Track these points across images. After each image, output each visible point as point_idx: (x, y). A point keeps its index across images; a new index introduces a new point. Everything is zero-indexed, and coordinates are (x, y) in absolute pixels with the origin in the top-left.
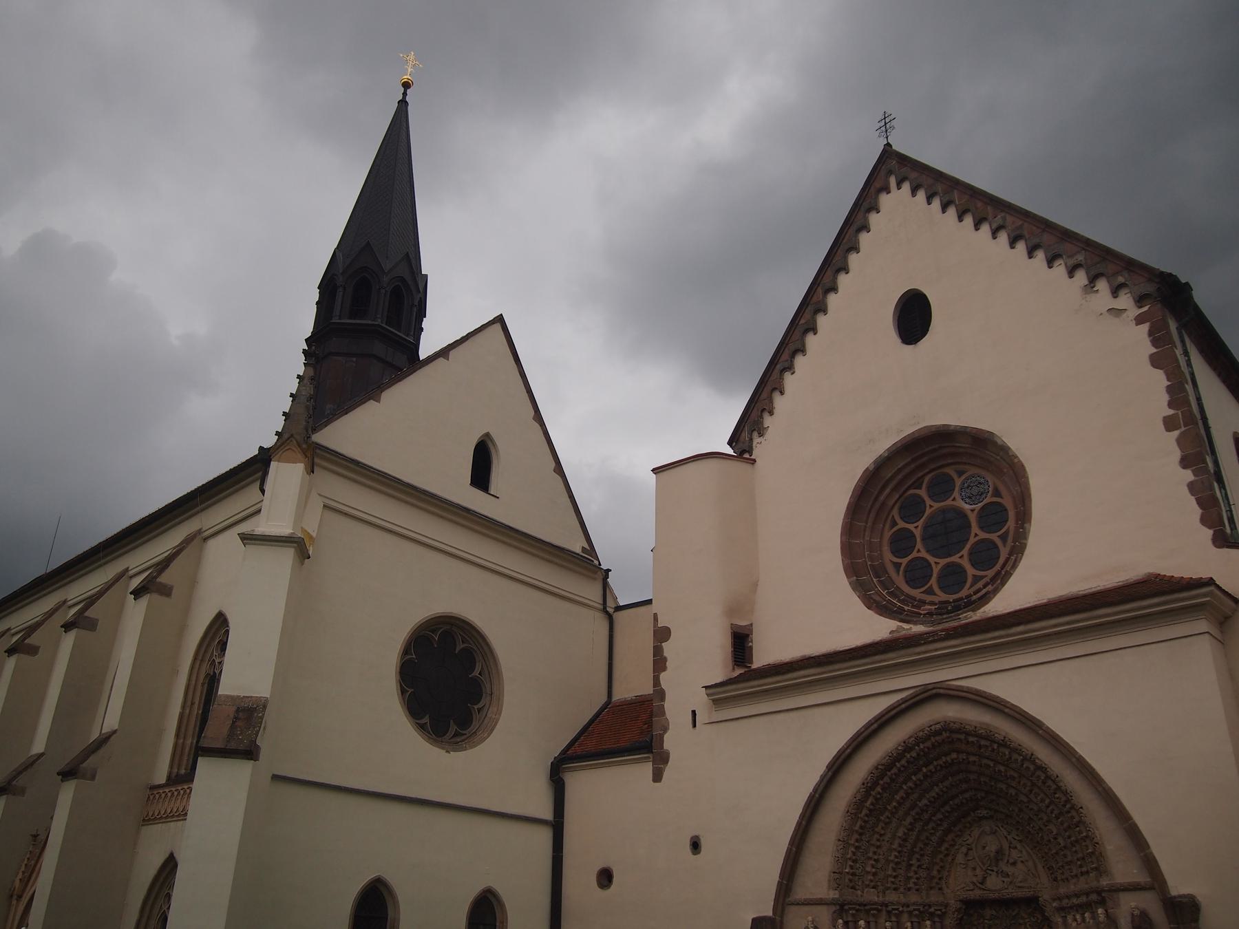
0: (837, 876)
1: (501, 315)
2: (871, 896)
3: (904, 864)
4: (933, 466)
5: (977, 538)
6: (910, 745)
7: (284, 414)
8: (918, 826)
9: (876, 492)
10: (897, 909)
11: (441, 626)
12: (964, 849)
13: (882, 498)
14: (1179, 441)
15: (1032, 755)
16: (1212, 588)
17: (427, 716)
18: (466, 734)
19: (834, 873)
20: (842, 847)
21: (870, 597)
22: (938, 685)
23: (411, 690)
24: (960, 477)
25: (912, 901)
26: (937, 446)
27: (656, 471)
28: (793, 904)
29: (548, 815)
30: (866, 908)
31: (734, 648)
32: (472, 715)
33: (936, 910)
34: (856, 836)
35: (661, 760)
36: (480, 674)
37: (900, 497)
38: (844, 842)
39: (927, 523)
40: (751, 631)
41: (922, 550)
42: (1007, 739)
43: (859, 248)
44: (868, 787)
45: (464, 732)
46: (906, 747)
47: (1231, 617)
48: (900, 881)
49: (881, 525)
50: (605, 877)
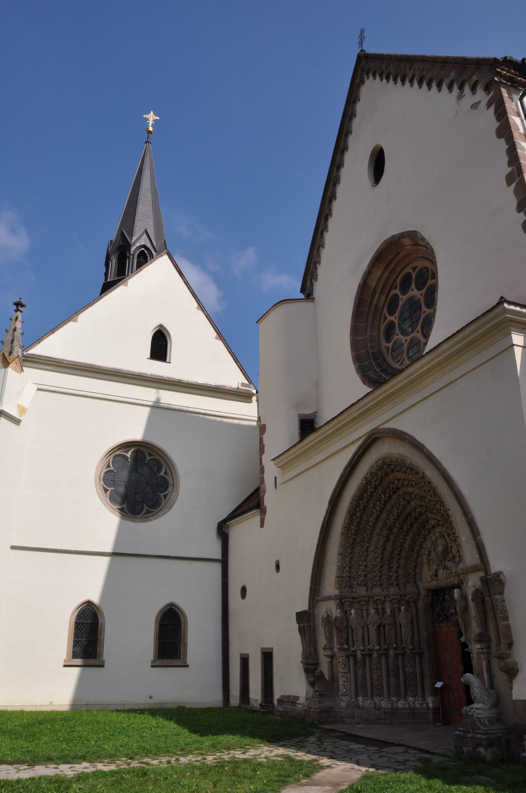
0: (339, 579)
2: (362, 591)
3: (386, 566)
4: (399, 269)
8: (392, 537)
10: (380, 600)
12: (427, 552)
13: (375, 302)
14: (516, 192)
15: (424, 473)
17: (126, 503)
19: (337, 577)
20: (341, 558)
24: (414, 271)
30: (358, 600)
31: (301, 430)
35: (263, 512)
36: (166, 473)
37: (387, 297)
39: (401, 312)
40: (316, 417)
42: (411, 464)
43: (352, 130)
44: (352, 513)
48: (384, 579)
49: (378, 322)
50: (244, 591)
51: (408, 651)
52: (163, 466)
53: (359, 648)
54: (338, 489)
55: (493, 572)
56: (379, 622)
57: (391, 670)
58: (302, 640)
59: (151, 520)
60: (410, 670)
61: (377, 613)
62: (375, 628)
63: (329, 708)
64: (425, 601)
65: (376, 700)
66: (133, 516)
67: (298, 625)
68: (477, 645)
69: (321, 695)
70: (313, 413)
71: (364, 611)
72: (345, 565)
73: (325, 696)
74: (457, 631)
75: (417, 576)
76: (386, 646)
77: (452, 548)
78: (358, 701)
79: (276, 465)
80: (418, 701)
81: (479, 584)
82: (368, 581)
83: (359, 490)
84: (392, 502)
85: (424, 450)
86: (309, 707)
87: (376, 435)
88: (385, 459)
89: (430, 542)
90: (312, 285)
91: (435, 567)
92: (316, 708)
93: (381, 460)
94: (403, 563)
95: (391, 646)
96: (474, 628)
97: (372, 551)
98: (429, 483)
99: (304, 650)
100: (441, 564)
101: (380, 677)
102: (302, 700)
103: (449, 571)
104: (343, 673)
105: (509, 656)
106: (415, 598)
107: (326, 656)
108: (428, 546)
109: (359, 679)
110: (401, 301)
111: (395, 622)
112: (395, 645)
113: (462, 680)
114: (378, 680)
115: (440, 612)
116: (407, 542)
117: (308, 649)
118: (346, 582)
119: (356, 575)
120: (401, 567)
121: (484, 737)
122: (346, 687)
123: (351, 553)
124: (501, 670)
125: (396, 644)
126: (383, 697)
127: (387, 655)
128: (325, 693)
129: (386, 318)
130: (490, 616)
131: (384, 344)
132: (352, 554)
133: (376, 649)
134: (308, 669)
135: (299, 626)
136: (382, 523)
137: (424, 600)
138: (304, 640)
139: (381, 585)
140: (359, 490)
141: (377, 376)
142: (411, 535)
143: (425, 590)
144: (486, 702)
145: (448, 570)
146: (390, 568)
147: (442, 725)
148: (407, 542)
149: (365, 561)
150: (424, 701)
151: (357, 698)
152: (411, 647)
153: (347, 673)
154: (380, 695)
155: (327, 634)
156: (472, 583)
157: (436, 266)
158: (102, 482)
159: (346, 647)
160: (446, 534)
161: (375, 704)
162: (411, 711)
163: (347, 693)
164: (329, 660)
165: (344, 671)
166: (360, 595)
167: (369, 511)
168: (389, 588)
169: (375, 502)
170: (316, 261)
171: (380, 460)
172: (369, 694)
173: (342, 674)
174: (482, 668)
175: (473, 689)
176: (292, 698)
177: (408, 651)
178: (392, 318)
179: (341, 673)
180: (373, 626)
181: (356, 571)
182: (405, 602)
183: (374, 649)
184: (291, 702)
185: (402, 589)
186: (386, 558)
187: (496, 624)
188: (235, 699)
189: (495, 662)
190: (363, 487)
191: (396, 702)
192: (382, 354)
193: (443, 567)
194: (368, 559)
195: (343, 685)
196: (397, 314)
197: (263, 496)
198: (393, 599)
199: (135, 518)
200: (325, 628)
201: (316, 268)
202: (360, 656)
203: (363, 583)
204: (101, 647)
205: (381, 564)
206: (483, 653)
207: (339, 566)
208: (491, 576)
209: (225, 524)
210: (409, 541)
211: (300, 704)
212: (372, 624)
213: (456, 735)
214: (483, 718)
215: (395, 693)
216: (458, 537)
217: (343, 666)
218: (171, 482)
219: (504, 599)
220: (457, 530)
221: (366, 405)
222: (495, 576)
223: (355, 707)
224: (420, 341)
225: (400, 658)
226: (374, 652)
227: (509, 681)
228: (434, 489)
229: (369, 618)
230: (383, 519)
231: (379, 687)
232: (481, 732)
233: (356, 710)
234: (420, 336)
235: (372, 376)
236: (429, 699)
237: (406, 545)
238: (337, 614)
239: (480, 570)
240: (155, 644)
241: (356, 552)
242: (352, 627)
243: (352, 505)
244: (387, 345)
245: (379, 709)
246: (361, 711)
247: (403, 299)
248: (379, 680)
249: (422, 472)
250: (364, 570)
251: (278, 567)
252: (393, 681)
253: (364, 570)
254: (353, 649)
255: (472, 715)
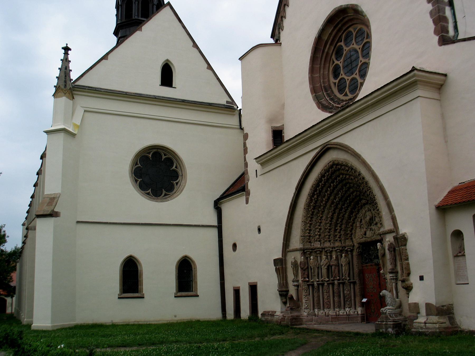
1: (169, 2)
2: (317, 245)
3: (333, 229)
4: (344, 28)
5: (362, 62)
6: (323, 174)
7: (57, 77)
8: (337, 211)
9: (322, 48)
10: (329, 250)
11: (152, 150)
12: (359, 220)
13: (326, 50)
15: (360, 172)
16: (415, 72)
17: (150, 189)
18: (171, 194)
19: (301, 236)
20: (304, 224)
21: (320, 103)
22: (327, 144)
23: (140, 180)
25: (336, 246)
26: (342, 18)
27: (241, 59)
28: (289, 252)
29: (216, 224)
30: (315, 250)
32: (174, 186)
33: (349, 249)
34: (309, 219)
35: (248, 194)
36: (176, 167)
37: (335, 47)
38: (305, 222)
40: (284, 128)
41: (343, 74)
42: (352, 165)
44: (311, 196)
45: (170, 193)
46: (322, 175)
47: (444, 84)
49: (328, 65)
50: (235, 246)
51: (347, 281)
52: (175, 163)
53: (315, 281)
54: (302, 180)
55: (401, 233)
56: (328, 264)
57: (335, 293)
58: (278, 276)
59: (169, 200)
60: (347, 292)
61: (327, 258)
62: (326, 267)
63: (297, 316)
64: (358, 250)
65: (326, 310)
66: (156, 198)
67: (275, 267)
68: (390, 275)
69: (292, 309)
70: (281, 126)
71: (319, 257)
72: (306, 228)
73: (294, 310)
74: (377, 268)
75: (353, 236)
76: (332, 278)
77: (375, 217)
78: (314, 312)
79: (257, 162)
80: (352, 310)
81: (392, 240)
82: (321, 238)
83: (317, 181)
84: (338, 188)
85: (361, 158)
86: (284, 317)
87: (329, 146)
88: (334, 161)
89: (362, 213)
90: (279, 33)
91: (365, 230)
92: (289, 317)
93: (332, 162)
94: (344, 227)
95: (335, 278)
96: (389, 265)
97: (324, 220)
98: (363, 178)
99: (279, 283)
100: (368, 227)
101: (328, 297)
102: (278, 313)
103: (373, 232)
104: (305, 295)
105: (408, 280)
106: (352, 248)
107: (294, 285)
108: (360, 216)
109: (316, 299)
110: (345, 51)
111: (339, 263)
112: (338, 278)
113: (381, 294)
114: (327, 299)
115: (367, 257)
116: (347, 214)
117: (282, 282)
118: (307, 239)
119: (313, 235)
120: (343, 230)
121: (392, 323)
122: (307, 304)
123: (310, 221)
124: (403, 287)
125: (339, 277)
126: (330, 309)
127: (333, 284)
128: (294, 308)
129: (334, 62)
130: (398, 258)
131: (332, 80)
132: (311, 222)
133: (326, 280)
134: (282, 294)
135: (275, 268)
136: (331, 202)
137: (357, 250)
138: (279, 277)
139: (330, 241)
140: (317, 181)
141: (328, 103)
142: (349, 209)
143: (357, 244)
144: (394, 306)
145: (373, 231)
146: (335, 230)
147: (366, 323)
148: (347, 214)
149: (319, 226)
150: (356, 310)
151: (314, 310)
152: (348, 278)
153: (308, 295)
154: (329, 308)
155: (295, 272)
156: (388, 239)
157: (370, 30)
158: (133, 175)
159: (307, 279)
160: (372, 209)
161: (325, 313)
162: (348, 316)
163: (308, 307)
164: (296, 288)
165: (306, 294)
166: (316, 248)
167: (322, 194)
168: (335, 243)
169: (327, 188)
170: (282, 15)
171: (331, 162)
172: (322, 308)
173: (305, 296)
174: (392, 288)
175: (387, 298)
176: (271, 313)
177: (347, 281)
178: (338, 63)
179: (304, 295)
180: (324, 266)
181: (314, 232)
182: (345, 251)
183: (325, 281)
184: (270, 315)
185: (343, 244)
186: (333, 224)
187: (401, 262)
188: (230, 314)
189: (400, 283)
190: (319, 179)
191: (338, 311)
192: (330, 88)
193: (370, 229)
194: (322, 225)
195: (306, 303)
196: (342, 60)
197: (248, 183)
198: (338, 249)
199: (158, 199)
200: (293, 269)
201: (282, 20)
202: (316, 285)
203: (318, 240)
204: (141, 285)
205: (330, 228)
206: (393, 279)
207: (303, 229)
208: (400, 236)
209: (219, 201)
210: (348, 213)
211: (277, 316)
212: (324, 265)
213: (376, 324)
214: (392, 314)
215: (338, 306)
216: (380, 212)
217: (305, 291)
218: (180, 174)
219: (406, 248)
220: (380, 208)
221: (322, 126)
222: (402, 235)
223: (313, 315)
224: (358, 81)
225: (341, 285)
226: (325, 282)
227: (407, 294)
228: (366, 182)
229: (322, 261)
230: (331, 200)
231: (328, 303)
232: (390, 321)
233: (313, 317)
234: (358, 77)
235: (324, 102)
236: (359, 309)
237: (346, 216)
238: (301, 259)
239: (393, 232)
240: (176, 283)
241: (313, 220)
242: (311, 267)
243: (311, 190)
244: (335, 81)
245: (328, 316)
246: (317, 317)
247: (346, 49)
248: (328, 299)
249: (359, 171)
250: (319, 232)
251: (259, 230)
252: (336, 299)
253: (319, 232)
254: (312, 280)
255: (386, 313)
